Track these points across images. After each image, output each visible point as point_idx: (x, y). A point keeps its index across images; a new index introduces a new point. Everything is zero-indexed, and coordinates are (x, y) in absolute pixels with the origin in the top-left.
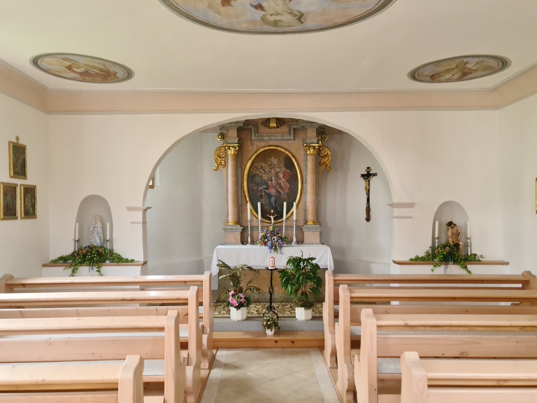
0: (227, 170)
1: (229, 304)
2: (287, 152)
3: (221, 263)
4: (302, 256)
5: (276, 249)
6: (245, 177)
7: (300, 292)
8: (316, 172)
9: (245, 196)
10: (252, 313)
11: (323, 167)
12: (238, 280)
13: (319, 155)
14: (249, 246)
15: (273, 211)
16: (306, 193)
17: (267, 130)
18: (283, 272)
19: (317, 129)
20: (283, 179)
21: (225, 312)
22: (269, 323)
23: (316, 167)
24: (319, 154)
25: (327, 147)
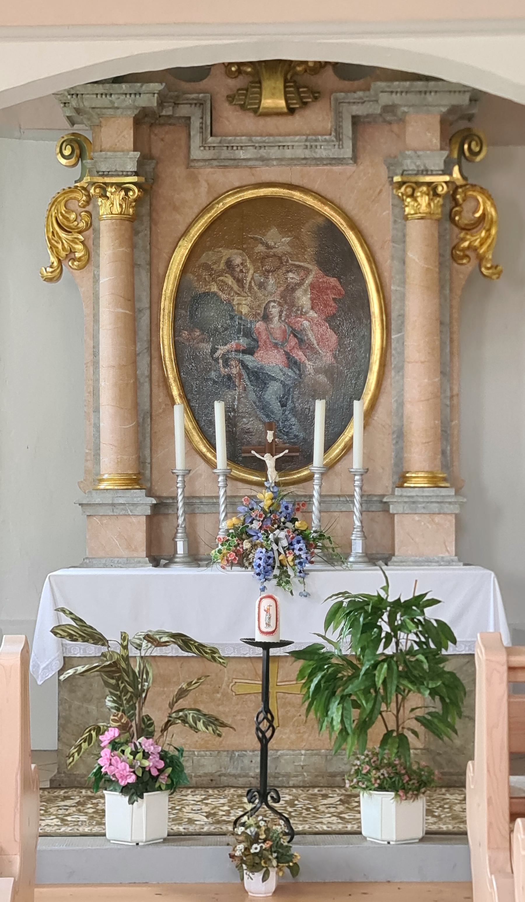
0: (96, 280)
1: (102, 781)
2: (327, 211)
3: (67, 620)
4: (386, 589)
5: (283, 579)
6: (166, 304)
7: (377, 731)
8: (442, 287)
9: (165, 380)
10: (191, 821)
11: (468, 267)
12: (135, 687)
13: (452, 220)
14: (178, 571)
15: (272, 444)
16: (400, 369)
17: (249, 123)
18: (311, 654)
19: (444, 122)
20: (312, 314)
21: (83, 818)
22: (255, 848)
23: (441, 265)
24: (451, 214)
25: (483, 191)
